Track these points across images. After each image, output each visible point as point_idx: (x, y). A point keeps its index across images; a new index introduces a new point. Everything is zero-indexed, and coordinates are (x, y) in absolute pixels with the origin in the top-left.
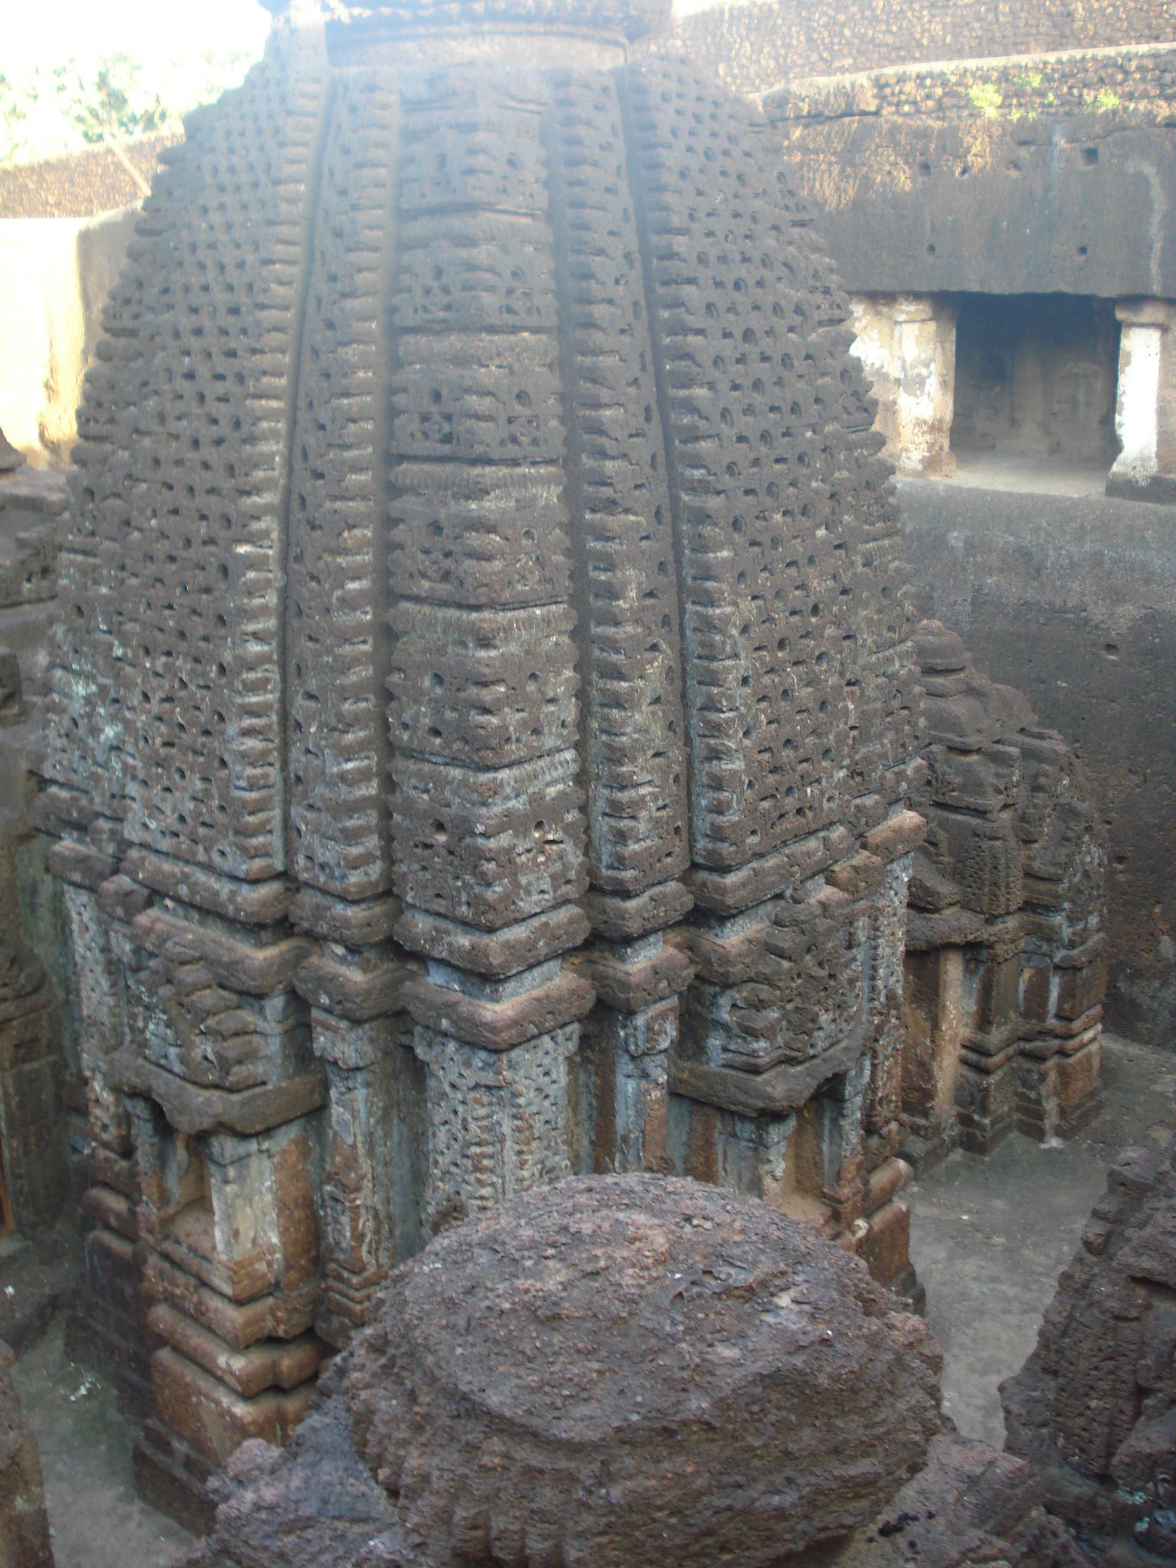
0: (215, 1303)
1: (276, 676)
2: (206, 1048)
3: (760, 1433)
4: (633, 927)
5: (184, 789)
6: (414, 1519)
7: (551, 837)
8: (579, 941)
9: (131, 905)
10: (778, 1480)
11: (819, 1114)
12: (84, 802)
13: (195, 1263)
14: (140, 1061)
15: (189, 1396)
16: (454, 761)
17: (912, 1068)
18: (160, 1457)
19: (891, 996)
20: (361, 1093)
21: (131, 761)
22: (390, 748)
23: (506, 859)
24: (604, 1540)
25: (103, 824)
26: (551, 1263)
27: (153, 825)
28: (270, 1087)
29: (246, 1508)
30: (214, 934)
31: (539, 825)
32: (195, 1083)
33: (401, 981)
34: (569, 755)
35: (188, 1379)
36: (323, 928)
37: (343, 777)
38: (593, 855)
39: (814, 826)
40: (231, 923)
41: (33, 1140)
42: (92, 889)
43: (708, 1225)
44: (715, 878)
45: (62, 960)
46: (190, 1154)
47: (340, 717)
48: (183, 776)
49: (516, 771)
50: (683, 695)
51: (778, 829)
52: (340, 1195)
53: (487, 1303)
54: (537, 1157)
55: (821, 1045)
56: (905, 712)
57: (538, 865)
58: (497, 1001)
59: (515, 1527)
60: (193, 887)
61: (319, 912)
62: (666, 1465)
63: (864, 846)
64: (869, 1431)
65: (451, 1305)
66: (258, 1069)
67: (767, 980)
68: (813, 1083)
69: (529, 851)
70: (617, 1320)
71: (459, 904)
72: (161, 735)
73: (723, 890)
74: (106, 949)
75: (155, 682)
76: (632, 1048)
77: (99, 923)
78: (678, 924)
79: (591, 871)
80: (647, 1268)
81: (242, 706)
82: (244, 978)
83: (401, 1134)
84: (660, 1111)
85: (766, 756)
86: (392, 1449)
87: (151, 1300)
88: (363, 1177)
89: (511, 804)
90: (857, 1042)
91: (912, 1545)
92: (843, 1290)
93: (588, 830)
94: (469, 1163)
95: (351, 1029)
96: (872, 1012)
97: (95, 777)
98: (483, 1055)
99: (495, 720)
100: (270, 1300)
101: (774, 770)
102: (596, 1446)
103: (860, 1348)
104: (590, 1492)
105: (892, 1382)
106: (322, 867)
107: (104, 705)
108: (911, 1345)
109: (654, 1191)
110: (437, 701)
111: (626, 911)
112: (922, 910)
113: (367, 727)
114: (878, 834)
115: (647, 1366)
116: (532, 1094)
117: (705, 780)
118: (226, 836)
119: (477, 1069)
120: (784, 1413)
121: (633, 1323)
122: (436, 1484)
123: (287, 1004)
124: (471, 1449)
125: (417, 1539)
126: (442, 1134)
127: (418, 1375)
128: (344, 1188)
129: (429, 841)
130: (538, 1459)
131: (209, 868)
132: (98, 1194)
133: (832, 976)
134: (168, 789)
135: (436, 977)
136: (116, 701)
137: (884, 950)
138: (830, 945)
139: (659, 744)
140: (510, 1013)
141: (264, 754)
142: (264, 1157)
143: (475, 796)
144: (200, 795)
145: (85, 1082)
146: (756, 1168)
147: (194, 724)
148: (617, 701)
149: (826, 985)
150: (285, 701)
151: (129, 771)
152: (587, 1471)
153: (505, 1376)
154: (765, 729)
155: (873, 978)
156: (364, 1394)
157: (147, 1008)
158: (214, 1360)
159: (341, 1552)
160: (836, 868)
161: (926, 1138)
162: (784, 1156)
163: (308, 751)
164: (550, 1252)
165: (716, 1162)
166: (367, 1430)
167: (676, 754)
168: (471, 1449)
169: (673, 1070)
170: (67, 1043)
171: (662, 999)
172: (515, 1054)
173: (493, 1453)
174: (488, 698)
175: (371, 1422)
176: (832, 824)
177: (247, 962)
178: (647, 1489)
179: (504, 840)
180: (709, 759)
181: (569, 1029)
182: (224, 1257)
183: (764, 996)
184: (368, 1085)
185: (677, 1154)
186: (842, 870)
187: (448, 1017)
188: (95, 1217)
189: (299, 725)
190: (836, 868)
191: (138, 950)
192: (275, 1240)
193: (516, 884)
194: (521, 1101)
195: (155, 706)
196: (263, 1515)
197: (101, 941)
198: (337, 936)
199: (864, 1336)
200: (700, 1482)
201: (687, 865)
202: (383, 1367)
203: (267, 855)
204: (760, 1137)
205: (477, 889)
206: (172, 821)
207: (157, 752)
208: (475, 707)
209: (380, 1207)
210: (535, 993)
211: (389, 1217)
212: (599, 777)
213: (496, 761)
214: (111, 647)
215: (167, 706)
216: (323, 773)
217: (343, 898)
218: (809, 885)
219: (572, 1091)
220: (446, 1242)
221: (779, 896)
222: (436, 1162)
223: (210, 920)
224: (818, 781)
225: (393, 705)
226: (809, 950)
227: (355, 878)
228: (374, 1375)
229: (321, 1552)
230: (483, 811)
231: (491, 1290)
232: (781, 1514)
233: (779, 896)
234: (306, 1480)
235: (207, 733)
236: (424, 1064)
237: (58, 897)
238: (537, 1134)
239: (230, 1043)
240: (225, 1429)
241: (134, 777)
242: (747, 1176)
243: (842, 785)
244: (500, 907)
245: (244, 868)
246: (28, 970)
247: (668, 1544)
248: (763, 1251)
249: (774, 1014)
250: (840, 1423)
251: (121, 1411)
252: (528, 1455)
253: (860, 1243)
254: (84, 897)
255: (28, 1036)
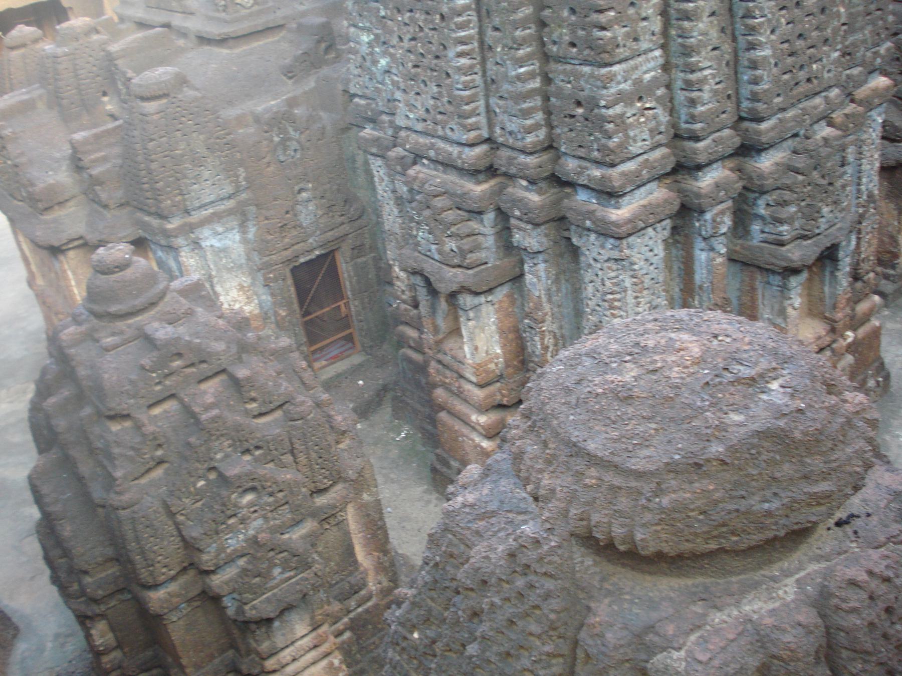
0: (468, 387)
1: (475, 19)
2: (451, 244)
3: (756, 466)
4: (702, 159)
5: (427, 92)
6: (547, 514)
7: (648, 105)
8: (668, 169)
9: (404, 164)
10: (768, 493)
11: (823, 268)
12: (374, 106)
13: (456, 365)
14: (417, 254)
15: (457, 437)
16: (585, 62)
17: (886, 239)
18: (445, 470)
19: (870, 196)
20: (542, 266)
21: (396, 78)
22: (546, 58)
23: (620, 121)
24: (659, 528)
25: (385, 118)
26: (628, 365)
27: (411, 116)
28: (489, 265)
29: (457, 506)
30: (452, 179)
31: (640, 99)
32: (447, 265)
33: (561, 199)
34: (658, 53)
35: (456, 428)
36: (513, 170)
37: (519, 77)
38: (675, 115)
39: (818, 89)
40: (461, 171)
41: (366, 300)
42: (383, 157)
43: (728, 340)
44: (754, 125)
45: (373, 199)
46: (449, 305)
47: (514, 40)
48: (426, 85)
49: (624, 66)
50: (730, 10)
51: (795, 92)
52: (533, 325)
53: (588, 389)
54: (647, 299)
55: (823, 227)
56: (879, 13)
57: (640, 123)
58: (618, 208)
59: (605, 520)
60: (438, 151)
61: (510, 160)
62: (697, 485)
63: (852, 101)
64: (827, 465)
65: (568, 391)
66: (482, 255)
67: (788, 188)
68: (817, 251)
69: (634, 115)
70: (668, 399)
71: (593, 151)
72: (411, 61)
73: (759, 133)
74: (394, 191)
75: (405, 29)
76: (704, 233)
77: (389, 176)
78: (731, 155)
79: (674, 126)
80: (687, 367)
81: (456, 38)
82: (470, 202)
83: (567, 289)
84: (722, 270)
85: (786, 45)
86: (534, 474)
87: (435, 386)
88: (546, 314)
89: (622, 86)
90: (847, 225)
91: (855, 532)
92: (813, 378)
93: (671, 100)
94: (606, 304)
95: (533, 229)
96: (858, 205)
97: (378, 90)
98: (612, 241)
99: (608, 34)
100: (498, 384)
101: (791, 54)
102: (652, 473)
103: (824, 414)
104: (649, 500)
105: (843, 436)
106: (511, 133)
107: (378, 47)
108: (857, 412)
109: (696, 320)
110: (572, 25)
111: (697, 149)
112: (893, 141)
113: (531, 45)
114: (861, 93)
115: (685, 426)
116: (642, 263)
117: (746, 63)
118: (453, 119)
119: (608, 249)
120: (772, 454)
121: (677, 400)
122: (559, 495)
123: (497, 216)
124: (579, 475)
125: (548, 526)
126: (590, 289)
127: (548, 433)
128: (535, 320)
129: (572, 113)
130: (618, 481)
131: (445, 139)
132: (402, 328)
133: (830, 184)
134: (418, 94)
135: (582, 196)
136: (384, 43)
137: (866, 167)
138: (829, 164)
139: (715, 42)
140: (627, 215)
141: (472, 67)
142: (489, 305)
143: (599, 83)
144: (436, 95)
145: (390, 266)
146: (782, 303)
147: (429, 52)
148: (687, 16)
149: (828, 190)
150: (481, 33)
151: (394, 83)
152: (647, 488)
153: (599, 432)
154: (784, 28)
155: (859, 184)
156: (518, 443)
157: (418, 223)
158: (469, 417)
159: (510, 531)
160: (833, 116)
161: (894, 282)
162: (800, 295)
163: (497, 63)
164: (628, 358)
165: (757, 299)
166: (521, 463)
167: (727, 47)
168: (579, 475)
169: (731, 246)
170: (380, 245)
171: (722, 202)
172: (631, 239)
173: (591, 477)
174: (604, 20)
175: (522, 459)
176: (830, 87)
177: (472, 193)
178: (685, 499)
179: (618, 109)
180: (748, 50)
181: (664, 223)
182: (470, 361)
183: (786, 198)
184: (545, 261)
185: (733, 295)
186: (837, 116)
187: (590, 219)
188: (402, 341)
189: (490, 48)
190: (833, 116)
191: (411, 190)
192: (499, 351)
193: (627, 137)
194: (636, 267)
195: (406, 44)
196: (467, 510)
197: (391, 186)
198: (521, 174)
199: (826, 408)
200: (717, 495)
201: (736, 118)
202: (530, 426)
203: (479, 129)
204: (785, 284)
205: (603, 141)
206: (422, 113)
207: (409, 71)
208: (596, 27)
209: (556, 331)
210: (642, 202)
211: (563, 336)
212: (677, 66)
213: (611, 60)
214: (378, 10)
215: (413, 42)
216: (507, 76)
217: (523, 152)
218: (816, 127)
219: (668, 261)
220: (567, 353)
221: (795, 135)
222: (588, 305)
223: (449, 170)
224: (820, 60)
225: (546, 30)
226: (815, 168)
227: (530, 139)
228: (524, 431)
229: (499, 531)
230: (604, 92)
231: (591, 381)
232: (769, 514)
233: (795, 135)
234: (491, 490)
235: (437, 57)
236: (578, 248)
237: (366, 163)
238: (646, 286)
239: (465, 241)
240: (478, 455)
241: (399, 88)
242: (777, 307)
243: (837, 62)
244: (618, 151)
245: (465, 137)
246: (355, 206)
247: (698, 531)
248: (762, 356)
249: (793, 209)
250: (808, 460)
251: (424, 445)
252: (611, 478)
253: (849, 346)
254: (379, 162)
255: (358, 243)
